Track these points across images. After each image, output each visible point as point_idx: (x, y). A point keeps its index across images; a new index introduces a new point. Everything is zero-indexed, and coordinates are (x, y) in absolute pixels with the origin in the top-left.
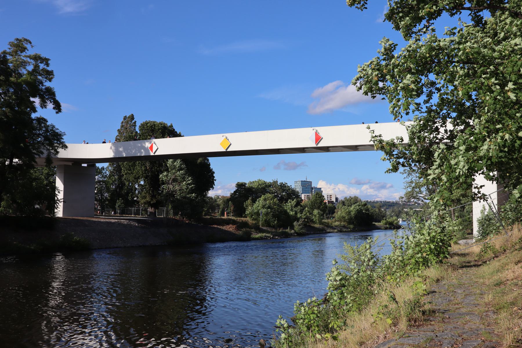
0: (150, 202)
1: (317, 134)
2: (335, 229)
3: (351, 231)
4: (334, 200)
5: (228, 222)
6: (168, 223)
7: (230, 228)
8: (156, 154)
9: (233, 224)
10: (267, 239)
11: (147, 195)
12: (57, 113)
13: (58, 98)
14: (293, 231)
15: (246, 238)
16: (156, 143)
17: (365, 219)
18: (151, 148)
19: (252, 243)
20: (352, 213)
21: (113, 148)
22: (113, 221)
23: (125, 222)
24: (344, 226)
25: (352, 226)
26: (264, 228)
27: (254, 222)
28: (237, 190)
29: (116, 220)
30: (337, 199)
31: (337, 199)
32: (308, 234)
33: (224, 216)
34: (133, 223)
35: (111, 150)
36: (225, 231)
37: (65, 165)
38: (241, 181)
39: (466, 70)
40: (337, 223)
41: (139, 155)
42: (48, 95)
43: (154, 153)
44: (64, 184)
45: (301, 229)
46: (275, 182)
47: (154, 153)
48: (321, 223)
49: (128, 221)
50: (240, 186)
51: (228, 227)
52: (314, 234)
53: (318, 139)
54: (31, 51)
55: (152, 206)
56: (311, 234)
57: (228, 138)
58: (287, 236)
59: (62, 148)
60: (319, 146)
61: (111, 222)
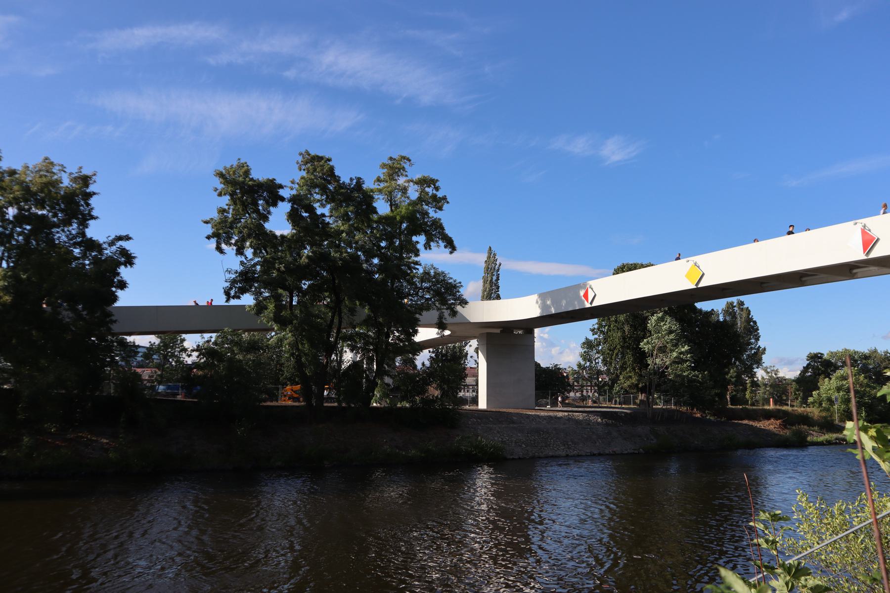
0: (637, 385)
1: (864, 232)
5: (768, 415)
6: (668, 417)
7: (771, 425)
8: (594, 304)
9: (777, 418)
10: (840, 444)
11: (632, 374)
12: (451, 253)
13: (449, 231)
15: (801, 443)
18: (586, 295)
19: (812, 450)
22: (560, 414)
23: (580, 416)
27: (824, 414)
28: (808, 365)
29: (566, 414)
34: (592, 418)
36: (760, 429)
37: (487, 333)
41: (570, 309)
42: (436, 233)
43: (591, 303)
47: (591, 303)
49: (585, 414)
50: (815, 358)
51: (767, 423)
53: (869, 242)
54: (415, 173)
55: (642, 390)
57: (699, 263)
59: (460, 304)
60: (873, 255)
61: (556, 417)
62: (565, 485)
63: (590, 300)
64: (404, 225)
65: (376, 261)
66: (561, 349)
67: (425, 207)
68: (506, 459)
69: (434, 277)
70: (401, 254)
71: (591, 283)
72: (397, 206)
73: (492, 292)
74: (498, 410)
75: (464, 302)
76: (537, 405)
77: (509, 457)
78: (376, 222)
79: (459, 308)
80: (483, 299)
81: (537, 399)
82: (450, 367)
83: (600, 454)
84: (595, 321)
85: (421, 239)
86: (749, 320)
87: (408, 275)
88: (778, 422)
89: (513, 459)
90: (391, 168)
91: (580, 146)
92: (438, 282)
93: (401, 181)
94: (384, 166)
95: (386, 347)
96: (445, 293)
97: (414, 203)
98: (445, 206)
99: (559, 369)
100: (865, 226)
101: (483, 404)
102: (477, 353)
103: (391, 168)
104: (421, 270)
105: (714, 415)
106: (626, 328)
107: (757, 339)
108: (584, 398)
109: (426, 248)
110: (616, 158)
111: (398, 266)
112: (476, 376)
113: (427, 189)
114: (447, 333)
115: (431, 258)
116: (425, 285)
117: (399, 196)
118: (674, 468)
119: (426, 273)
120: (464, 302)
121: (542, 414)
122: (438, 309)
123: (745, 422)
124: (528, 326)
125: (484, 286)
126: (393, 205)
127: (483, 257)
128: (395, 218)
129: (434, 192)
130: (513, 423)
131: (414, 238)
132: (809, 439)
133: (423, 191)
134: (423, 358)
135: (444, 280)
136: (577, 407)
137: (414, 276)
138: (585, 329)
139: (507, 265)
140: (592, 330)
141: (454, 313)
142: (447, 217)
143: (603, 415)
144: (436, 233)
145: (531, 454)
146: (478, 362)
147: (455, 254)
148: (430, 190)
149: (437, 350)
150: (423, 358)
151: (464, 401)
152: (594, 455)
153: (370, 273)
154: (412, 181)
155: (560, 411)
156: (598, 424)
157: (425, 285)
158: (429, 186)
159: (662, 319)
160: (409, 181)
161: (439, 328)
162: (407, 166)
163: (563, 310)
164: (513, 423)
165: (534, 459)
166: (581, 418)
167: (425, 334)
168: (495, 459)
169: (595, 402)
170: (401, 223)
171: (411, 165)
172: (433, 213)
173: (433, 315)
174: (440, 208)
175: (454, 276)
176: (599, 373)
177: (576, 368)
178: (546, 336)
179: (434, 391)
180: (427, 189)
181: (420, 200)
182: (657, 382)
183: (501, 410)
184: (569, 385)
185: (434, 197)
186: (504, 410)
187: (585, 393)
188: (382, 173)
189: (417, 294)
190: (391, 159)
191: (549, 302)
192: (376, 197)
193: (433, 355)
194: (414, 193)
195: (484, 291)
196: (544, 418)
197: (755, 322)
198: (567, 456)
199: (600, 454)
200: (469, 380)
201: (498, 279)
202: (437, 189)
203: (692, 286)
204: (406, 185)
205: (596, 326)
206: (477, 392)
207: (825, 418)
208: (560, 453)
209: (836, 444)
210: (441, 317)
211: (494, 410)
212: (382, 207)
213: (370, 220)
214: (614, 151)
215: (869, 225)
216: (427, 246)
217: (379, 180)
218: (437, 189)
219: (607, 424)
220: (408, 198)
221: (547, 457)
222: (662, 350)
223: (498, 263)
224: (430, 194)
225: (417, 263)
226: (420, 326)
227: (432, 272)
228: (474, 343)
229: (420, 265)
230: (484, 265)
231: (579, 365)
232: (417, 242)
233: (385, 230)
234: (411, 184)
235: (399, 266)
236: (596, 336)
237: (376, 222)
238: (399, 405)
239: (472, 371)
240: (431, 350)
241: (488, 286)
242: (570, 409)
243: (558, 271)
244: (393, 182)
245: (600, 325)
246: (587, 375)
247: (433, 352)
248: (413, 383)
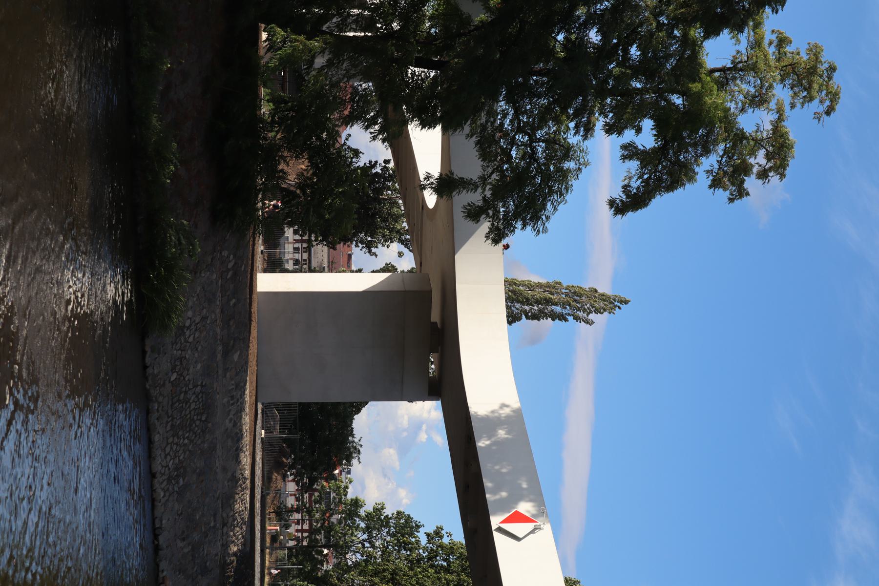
8: (497, 536)
12: (612, 203)
13: (661, 202)
16: (538, 534)
18: (518, 518)
21: (507, 411)
22: (246, 460)
23: (241, 506)
29: (247, 473)
34: (238, 533)
35: (496, 407)
37: (430, 292)
39: (769, 165)
41: (488, 484)
42: (661, 172)
43: (500, 530)
44: (364, 292)
47: (500, 530)
49: (246, 515)
54: (800, 123)
61: (238, 450)
62: (89, 472)
63: (507, 527)
64: (678, 100)
65: (594, 36)
67: (721, 147)
68: (143, 336)
69: (559, 170)
70: (612, 93)
71: (547, 528)
72: (722, 85)
73: (525, 303)
74: (255, 317)
75: (497, 236)
76: (267, 408)
77: (149, 343)
78: (685, 35)
79: (485, 226)
80: (509, 283)
81: (277, 406)
82: (350, 209)
83: (156, 534)
84: (459, 537)
85: (646, 137)
87: (564, 110)
89: (144, 353)
90: (812, 71)
92: (547, 177)
93: (781, 93)
94: (815, 52)
95: (396, 60)
96: (521, 194)
97: (728, 121)
98: (722, 195)
99: (349, 458)
101: (267, 283)
102: (383, 270)
103: (812, 71)
104: (573, 139)
108: (282, 514)
109: (624, 147)
111: (580, 88)
112: (333, 267)
113: (762, 153)
114: (431, 199)
115: (603, 160)
116: (540, 148)
117: (745, 87)
118: (114, 289)
119: (567, 152)
121: (247, 419)
122: (484, 179)
124: (445, 386)
125: (540, 285)
126: (726, 76)
127: (604, 288)
128: (694, 81)
129: (755, 170)
130: (226, 353)
131: (648, 124)
133: (758, 143)
134: (367, 146)
135: (551, 193)
136: (263, 498)
137: (558, 121)
138: (438, 513)
139: (587, 337)
140: (438, 533)
141: (474, 214)
143: (246, 557)
145: (154, 393)
146: (362, 273)
147: (606, 212)
148: (759, 159)
149: (391, 178)
150: (367, 146)
151: (274, 240)
152: (156, 536)
153: (566, 21)
154: (780, 118)
155: (250, 460)
156: (225, 546)
157: (540, 148)
158: (769, 156)
160: (780, 111)
161: (441, 179)
162: (815, 106)
164: (226, 353)
165: (144, 402)
166: (238, 507)
167: (427, 146)
168: (145, 315)
169: (274, 538)
170: (683, 93)
171: (818, 117)
172: (709, 163)
173: (472, 167)
174: (716, 183)
175: (560, 216)
176: (341, 549)
177: (351, 495)
178: (423, 437)
179: (295, 169)
180: (762, 153)
181: (740, 137)
183: (254, 324)
184: (313, 481)
185: (746, 169)
187: (297, 516)
188: (798, 48)
189: (520, 130)
190: (832, 69)
191: (502, 433)
192: (743, 37)
193: (378, 170)
194: (754, 122)
195: (530, 286)
196: (237, 423)
198: (153, 476)
199: (157, 549)
200: (321, 252)
201: (554, 316)
202: (763, 175)
204: (773, 105)
205: (446, 540)
206: (295, 271)
208: (159, 460)
210: (464, 184)
211: (255, 308)
212: (719, 50)
213: (686, 22)
216: (630, 152)
217: (782, 41)
218: (763, 175)
219: (224, 565)
220: (743, 110)
221: (149, 429)
223: (592, 316)
224: (752, 161)
225: (588, 130)
226: (444, 130)
227: (570, 165)
228: (407, 263)
229: (585, 138)
230: (586, 286)
232: (639, 130)
233: (668, 57)
234: (774, 117)
235: (582, 90)
236: (424, 540)
237: (685, 35)
238: (263, 91)
239: (343, 260)
240: (391, 165)
241: (538, 294)
242: (258, 482)
243: (572, 457)
244: (777, 74)
245: (451, 549)
246: (337, 518)
247: (385, 169)
248: (311, 123)
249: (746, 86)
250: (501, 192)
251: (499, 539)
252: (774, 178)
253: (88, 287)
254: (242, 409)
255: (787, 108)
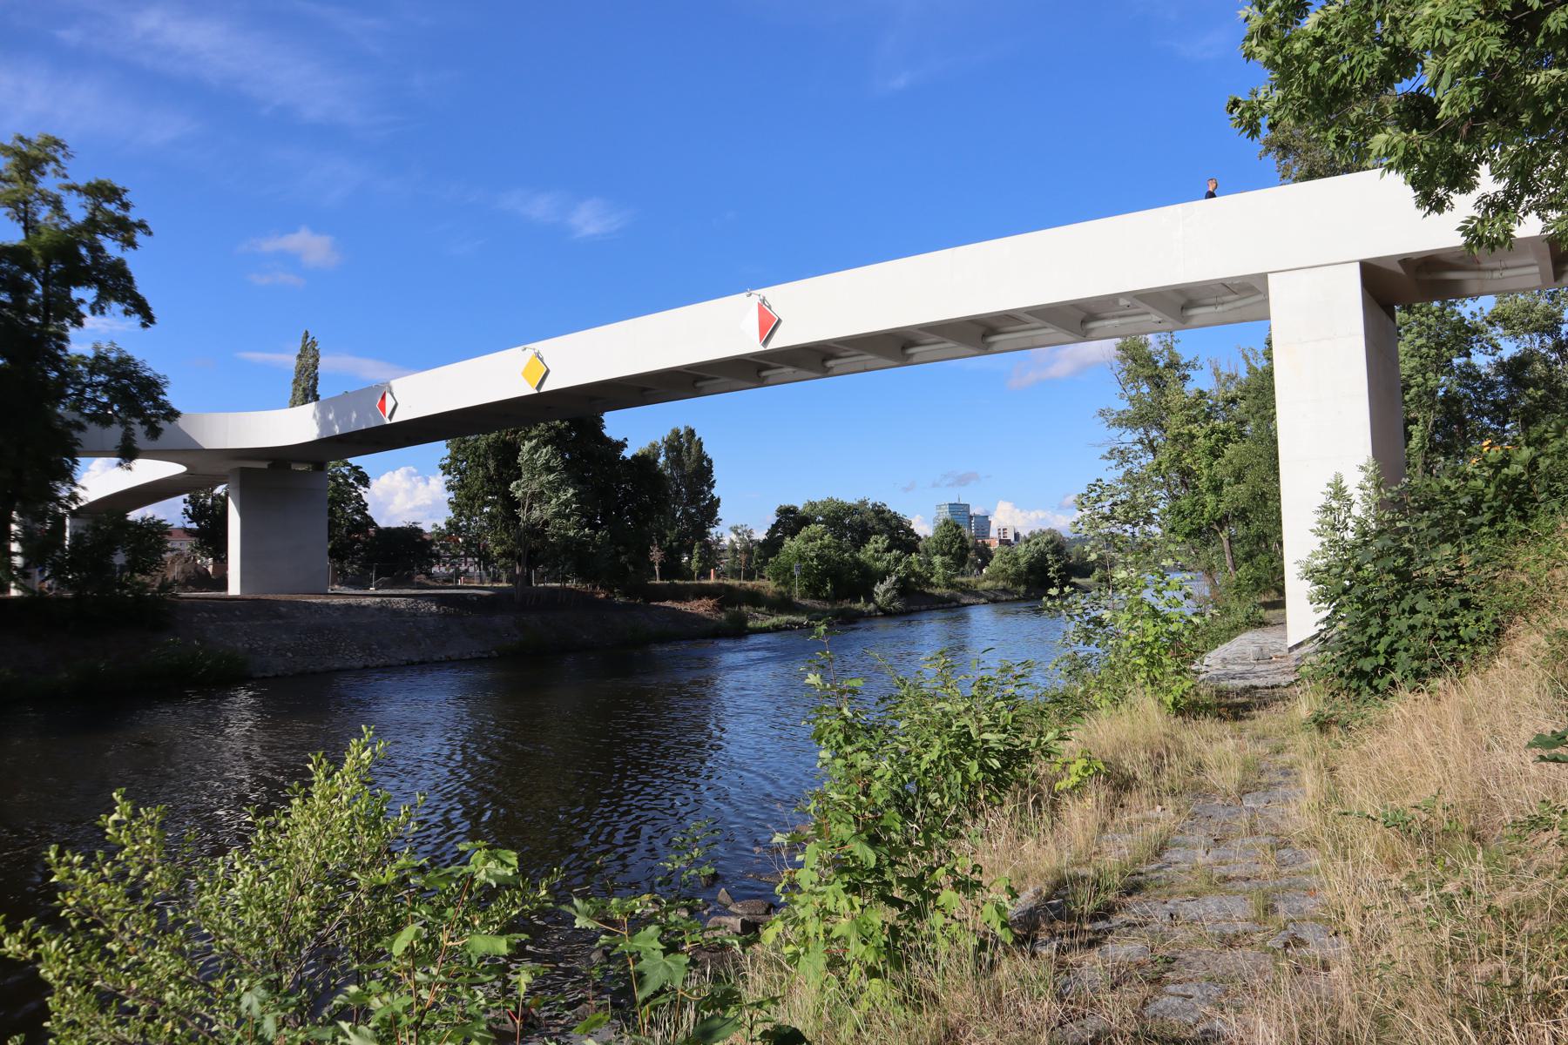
2: (981, 596)
3: (1019, 600)
4: (1011, 537)
7: (700, 607)
13: (142, 289)
14: (872, 606)
17: (1045, 575)
20: (1022, 561)
23: (402, 604)
24: (1004, 590)
25: (1022, 589)
26: (807, 602)
30: (1017, 536)
31: (1017, 536)
32: (911, 612)
33: (707, 576)
36: (685, 614)
38: (787, 503)
40: (988, 584)
42: (117, 286)
45: (891, 601)
46: (864, 503)
47: (390, 417)
48: (950, 585)
50: (786, 513)
51: (696, 603)
52: (928, 609)
53: (768, 325)
56: (920, 611)
57: (543, 354)
58: (849, 620)
61: (361, 608)
66: (408, 493)
79: (163, 424)
85: (84, 294)
86: (702, 457)
88: (711, 602)
91: (540, 208)
100: (763, 301)
105: (625, 595)
106: (491, 464)
107: (711, 486)
110: (590, 230)
116: (97, 379)
118: (244, 697)
120: (173, 414)
122: (123, 423)
123: (668, 603)
130: (280, 616)
131: (76, 293)
132: (750, 624)
133: (97, 207)
142: (142, 264)
144: (117, 286)
154: (75, 188)
156: (432, 614)
159: (535, 449)
160: (70, 188)
163: (352, 428)
164: (280, 616)
181: (92, 225)
182: (533, 548)
186: (270, 597)
190: (21, 139)
191: (331, 417)
194: (77, 210)
196: (337, 608)
197: (710, 462)
199: (422, 663)
202: (126, 206)
203: (526, 389)
207: (781, 593)
209: (786, 629)
214: (590, 220)
215: (769, 300)
219: (446, 615)
220: (67, 218)
222: (537, 497)
231: (449, 524)
232: (82, 301)
249: (44, 214)
250: (139, 413)
251: (397, 418)
252: (125, 198)
253: (240, 715)
254: (327, 605)
255: (67, 182)
